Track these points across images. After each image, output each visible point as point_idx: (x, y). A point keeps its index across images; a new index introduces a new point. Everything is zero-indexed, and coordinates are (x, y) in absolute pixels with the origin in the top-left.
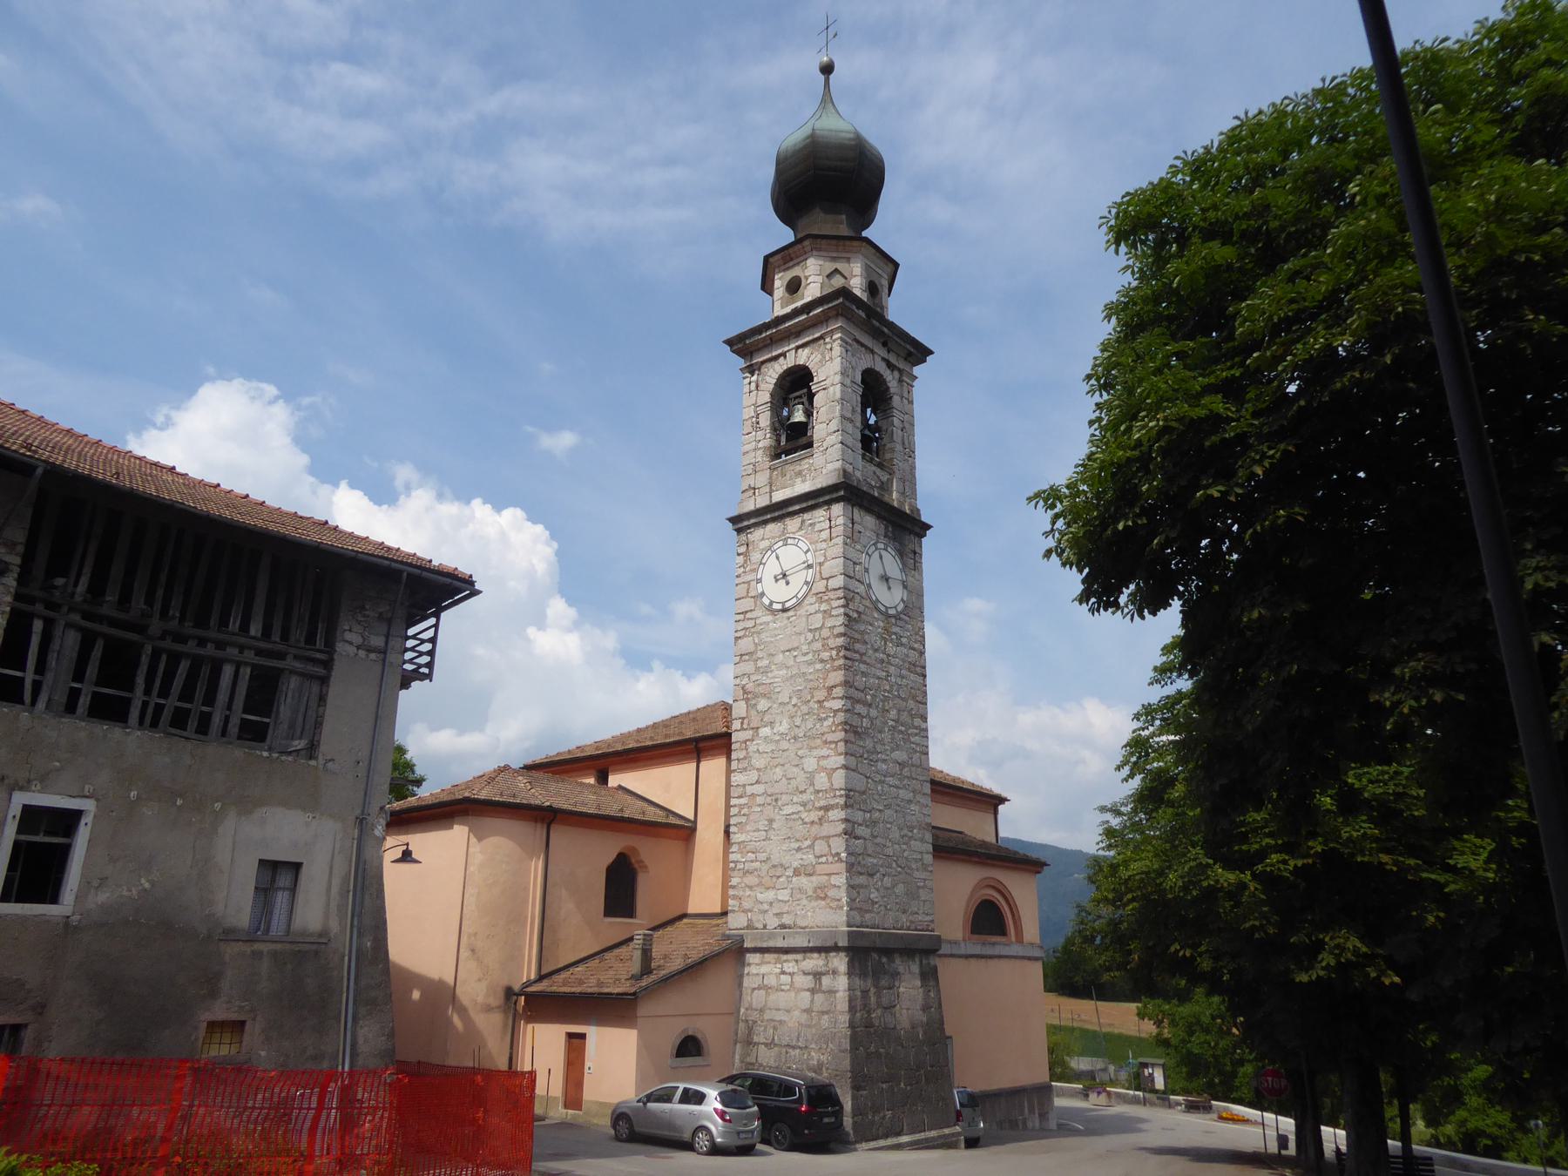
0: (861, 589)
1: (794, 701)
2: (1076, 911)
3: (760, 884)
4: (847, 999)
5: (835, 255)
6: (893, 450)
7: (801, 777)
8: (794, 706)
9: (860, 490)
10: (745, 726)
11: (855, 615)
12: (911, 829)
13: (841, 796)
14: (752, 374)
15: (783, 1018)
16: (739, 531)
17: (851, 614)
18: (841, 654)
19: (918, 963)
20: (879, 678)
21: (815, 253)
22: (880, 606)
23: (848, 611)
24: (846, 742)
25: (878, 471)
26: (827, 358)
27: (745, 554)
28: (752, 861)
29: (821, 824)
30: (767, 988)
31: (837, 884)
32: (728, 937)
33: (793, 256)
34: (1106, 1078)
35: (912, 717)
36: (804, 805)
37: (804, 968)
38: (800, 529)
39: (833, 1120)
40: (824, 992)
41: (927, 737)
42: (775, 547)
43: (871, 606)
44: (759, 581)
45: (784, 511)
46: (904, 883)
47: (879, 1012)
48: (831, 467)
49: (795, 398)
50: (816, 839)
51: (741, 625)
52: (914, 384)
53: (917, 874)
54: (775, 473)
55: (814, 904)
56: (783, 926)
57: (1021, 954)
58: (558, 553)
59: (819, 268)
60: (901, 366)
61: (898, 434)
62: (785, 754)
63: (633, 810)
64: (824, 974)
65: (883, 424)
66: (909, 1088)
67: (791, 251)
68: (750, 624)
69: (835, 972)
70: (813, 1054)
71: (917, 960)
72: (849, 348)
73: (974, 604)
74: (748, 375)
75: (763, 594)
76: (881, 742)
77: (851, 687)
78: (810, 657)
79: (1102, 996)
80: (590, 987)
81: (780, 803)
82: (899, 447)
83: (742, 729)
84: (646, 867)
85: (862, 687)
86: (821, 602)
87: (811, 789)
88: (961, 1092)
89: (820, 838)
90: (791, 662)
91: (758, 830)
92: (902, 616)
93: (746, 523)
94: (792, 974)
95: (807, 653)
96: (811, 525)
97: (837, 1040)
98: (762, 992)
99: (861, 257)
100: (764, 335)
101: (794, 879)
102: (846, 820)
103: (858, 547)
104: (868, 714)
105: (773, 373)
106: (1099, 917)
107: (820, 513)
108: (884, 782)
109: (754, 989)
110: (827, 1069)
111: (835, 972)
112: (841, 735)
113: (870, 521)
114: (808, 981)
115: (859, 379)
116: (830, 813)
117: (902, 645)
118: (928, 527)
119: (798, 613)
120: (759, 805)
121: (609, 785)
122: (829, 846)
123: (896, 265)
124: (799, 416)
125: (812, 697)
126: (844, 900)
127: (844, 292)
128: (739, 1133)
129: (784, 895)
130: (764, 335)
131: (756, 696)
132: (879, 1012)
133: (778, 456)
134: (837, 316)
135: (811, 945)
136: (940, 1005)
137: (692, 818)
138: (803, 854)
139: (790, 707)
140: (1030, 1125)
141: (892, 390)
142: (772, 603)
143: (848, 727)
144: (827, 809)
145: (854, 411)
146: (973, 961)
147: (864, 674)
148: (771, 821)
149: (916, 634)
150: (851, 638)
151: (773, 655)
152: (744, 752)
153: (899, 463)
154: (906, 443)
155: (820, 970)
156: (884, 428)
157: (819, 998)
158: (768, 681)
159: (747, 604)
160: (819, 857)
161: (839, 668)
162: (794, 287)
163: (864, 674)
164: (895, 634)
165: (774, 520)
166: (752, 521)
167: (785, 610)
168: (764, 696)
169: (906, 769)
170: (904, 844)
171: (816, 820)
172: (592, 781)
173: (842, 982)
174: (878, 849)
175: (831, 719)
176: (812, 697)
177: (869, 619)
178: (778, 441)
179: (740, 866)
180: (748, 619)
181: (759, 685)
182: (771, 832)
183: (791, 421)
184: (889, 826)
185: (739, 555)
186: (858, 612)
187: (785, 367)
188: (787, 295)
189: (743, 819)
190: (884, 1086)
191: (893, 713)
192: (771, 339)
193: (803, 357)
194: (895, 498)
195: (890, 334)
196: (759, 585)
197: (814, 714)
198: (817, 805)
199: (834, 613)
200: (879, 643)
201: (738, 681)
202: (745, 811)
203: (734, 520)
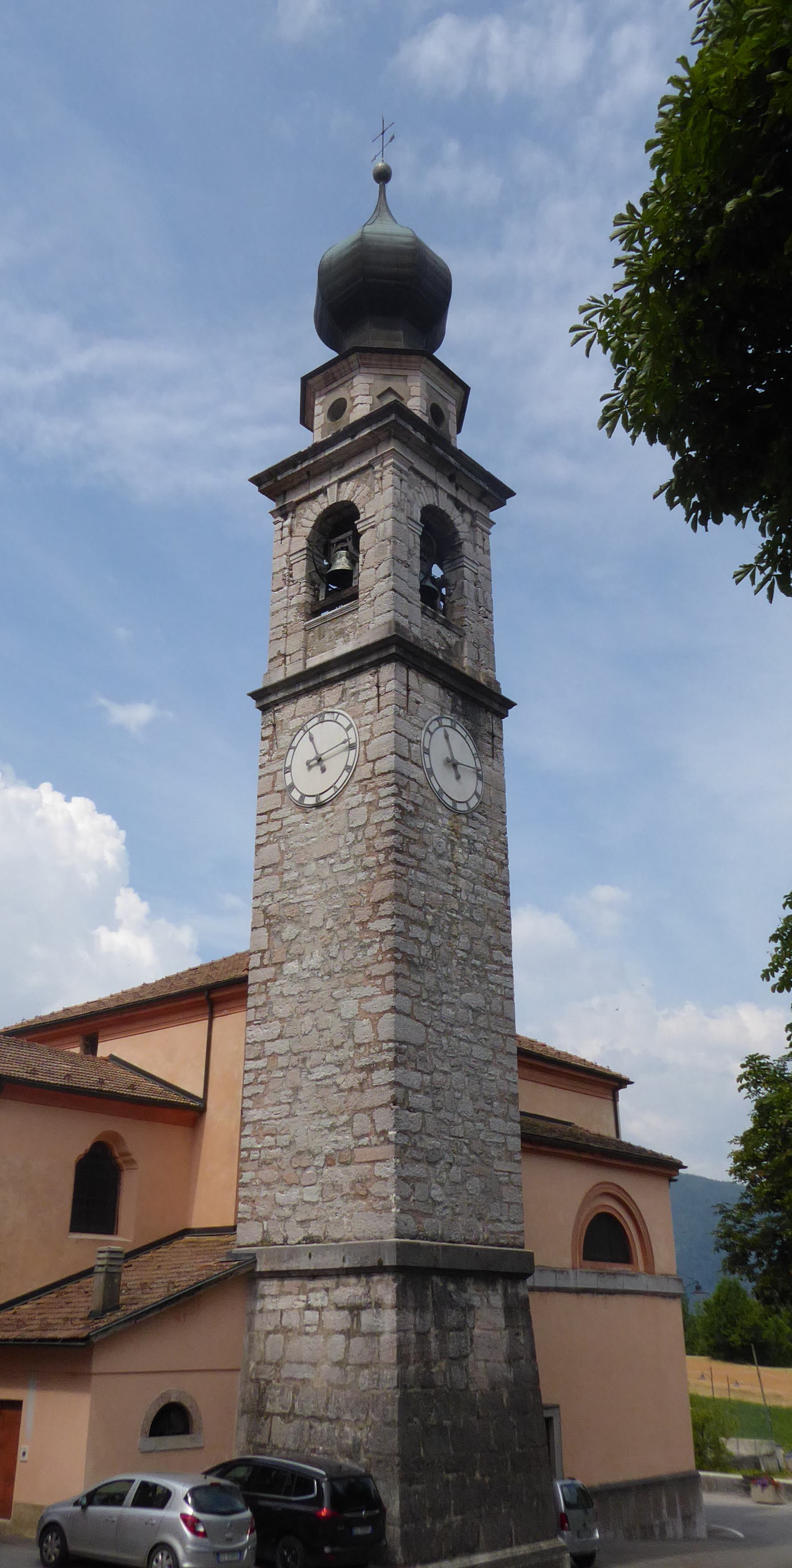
0: (418, 774)
1: (330, 924)
2: (720, 1217)
3: (281, 1180)
4: (395, 1344)
5: (389, 372)
6: (463, 607)
7: (337, 1026)
8: (330, 930)
9: (417, 647)
10: (266, 962)
11: (410, 808)
12: (489, 1101)
13: (389, 1050)
14: (285, 516)
15: (306, 1376)
16: (264, 709)
17: (405, 805)
18: (391, 858)
19: (500, 1291)
20: (444, 893)
21: (363, 370)
22: (445, 798)
23: (400, 801)
24: (397, 975)
25: (444, 632)
26: (377, 490)
27: (271, 738)
28: (270, 1148)
29: (362, 1091)
30: (286, 1331)
31: (384, 1175)
32: (236, 1257)
33: (337, 375)
34: (772, 1465)
35: (491, 947)
36: (340, 1065)
37: (337, 1300)
38: (341, 700)
39: (368, 1530)
40: (363, 1335)
41: (511, 976)
42: (309, 725)
43: (433, 798)
44: (288, 770)
45: (320, 680)
46: (479, 1176)
47: (443, 1364)
48: (380, 620)
49: (338, 543)
50: (356, 1111)
51: (265, 828)
52: (491, 530)
53: (498, 1165)
54: (312, 634)
55: (351, 1205)
56: (309, 1239)
57: (652, 1289)
58: (128, 843)
59: (368, 386)
60: (474, 508)
61: (469, 589)
62: (319, 995)
63: (120, 1082)
64: (364, 1308)
65: (452, 578)
66: (487, 1479)
67: (334, 369)
68: (275, 826)
69: (379, 1305)
70: (347, 1429)
71: (499, 1287)
72: (404, 476)
73: (605, 893)
74: (279, 519)
75: (292, 786)
76: (447, 978)
77: (404, 902)
78: (351, 863)
79: (766, 1360)
80: (32, 1332)
81: (308, 1064)
82: (471, 605)
83: (263, 966)
84: (133, 1162)
85: (420, 904)
86: (366, 792)
87: (350, 1043)
88: (568, 1486)
89: (359, 1111)
90: (326, 873)
91: (281, 1103)
92: (476, 815)
93: (273, 698)
94: (320, 1309)
95: (348, 859)
96: (354, 694)
97: (381, 1408)
98: (280, 1337)
99: (421, 374)
100: (299, 468)
101: (326, 1171)
102: (395, 1084)
103: (415, 721)
104: (428, 940)
105: (310, 514)
106: (753, 1226)
107: (366, 679)
108: (450, 1033)
109: (269, 1333)
110: (367, 1451)
111: (379, 1305)
112: (389, 966)
113: (431, 689)
114: (337, 1319)
115: (417, 516)
116: (375, 1075)
117: (476, 851)
118: (511, 704)
119: (336, 807)
120: (282, 1068)
121: (99, 1055)
122: (373, 1121)
123: (466, 389)
124: (341, 563)
125: (353, 917)
126: (392, 1197)
127: (398, 408)
128: (218, 1553)
129: (311, 1194)
130: (299, 468)
131: (281, 921)
132: (443, 1364)
133: (316, 613)
134: (388, 439)
135: (346, 1265)
136: (534, 1356)
137: (200, 1094)
138: (338, 1134)
139: (324, 932)
140: (670, 1532)
141: (462, 535)
142: (303, 796)
143: (399, 956)
144: (370, 1069)
145: (410, 553)
146: (586, 1297)
147: (422, 886)
148: (296, 1089)
149: (495, 839)
150: (405, 837)
151: (302, 865)
152: (264, 997)
153: (471, 623)
154: (481, 600)
155: (358, 1302)
156: (453, 581)
157: (357, 1343)
158: (297, 900)
159: (273, 801)
160: (358, 1138)
161: (388, 876)
162: (337, 410)
163: (422, 886)
164: (466, 836)
165: (307, 692)
166: (281, 695)
167: (319, 805)
168: (291, 919)
169: (481, 1018)
170: (481, 1121)
171: (356, 1084)
172: (77, 1050)
173: (388, 1320)
174: (444, 1127)
175: (377, 946)
176: (353, 917)
177: (429, 814)
178: (316, 597)
179: (254, 1155)
180: (274, 820)
181: (285, 905)
182: (297, 1105)
183: (333, 569)
184: (458, 1095)
185: (263, 739)
186: (414, 804)
187: (325, 506)
188: (329, 421)
189: (260, 1089)
190: (450, 1477)
191: (464, 941)
192: (308, 473)
193: (347, 492)
194: (466, 665)
195: (458, 465)
196: (288, 775)
197: (356, 940)
198: (358, 1064)
199: (382, 804)
200: (444, 847)
201: (258, 902)
202: (263, 1077)
203: (257, 695)
